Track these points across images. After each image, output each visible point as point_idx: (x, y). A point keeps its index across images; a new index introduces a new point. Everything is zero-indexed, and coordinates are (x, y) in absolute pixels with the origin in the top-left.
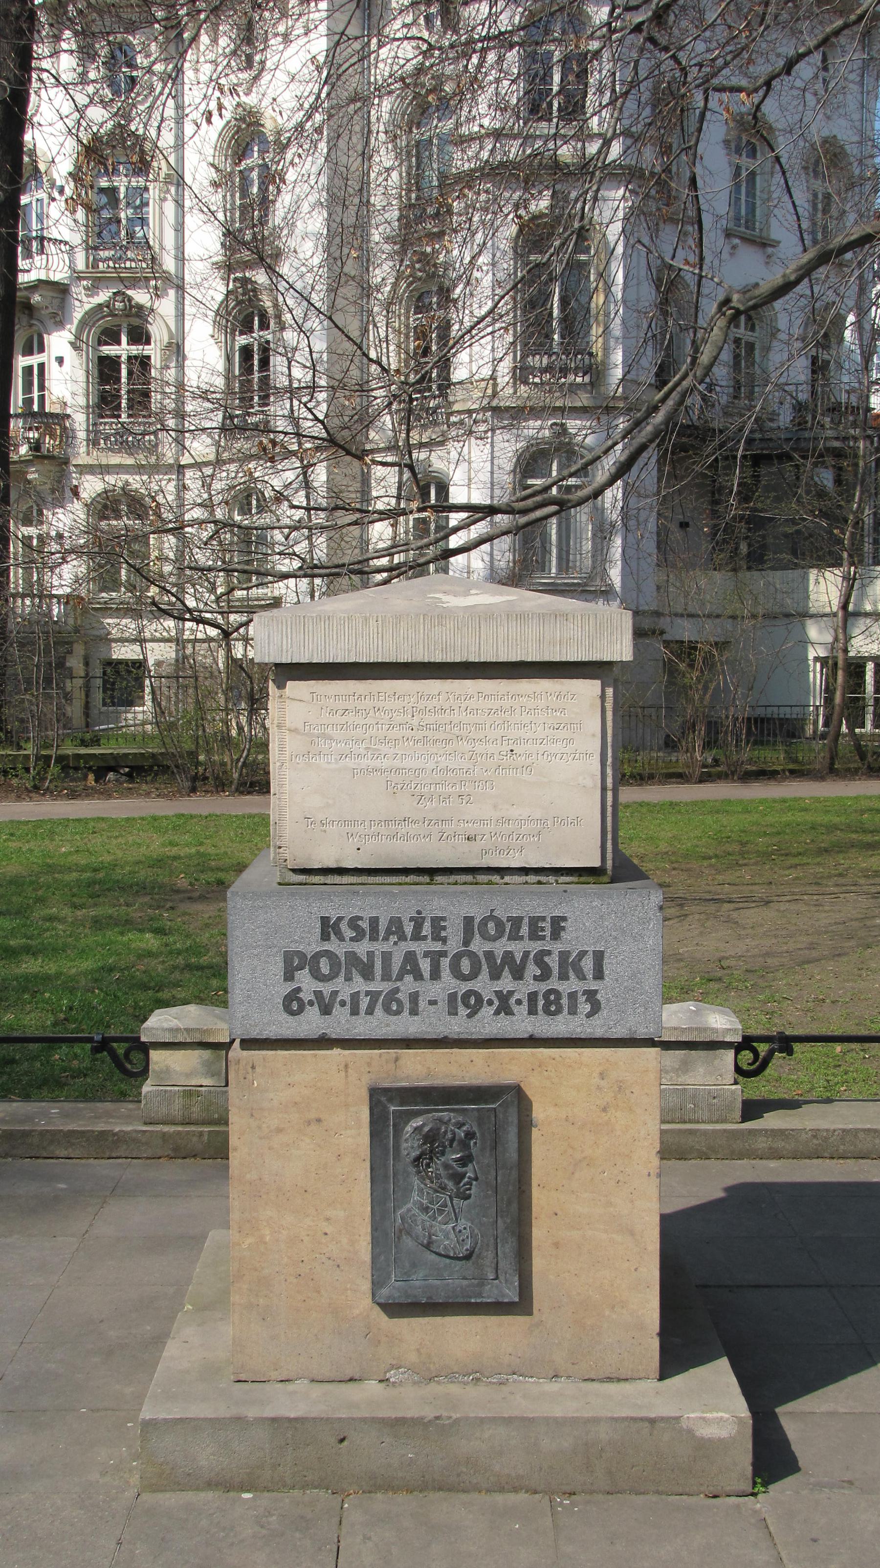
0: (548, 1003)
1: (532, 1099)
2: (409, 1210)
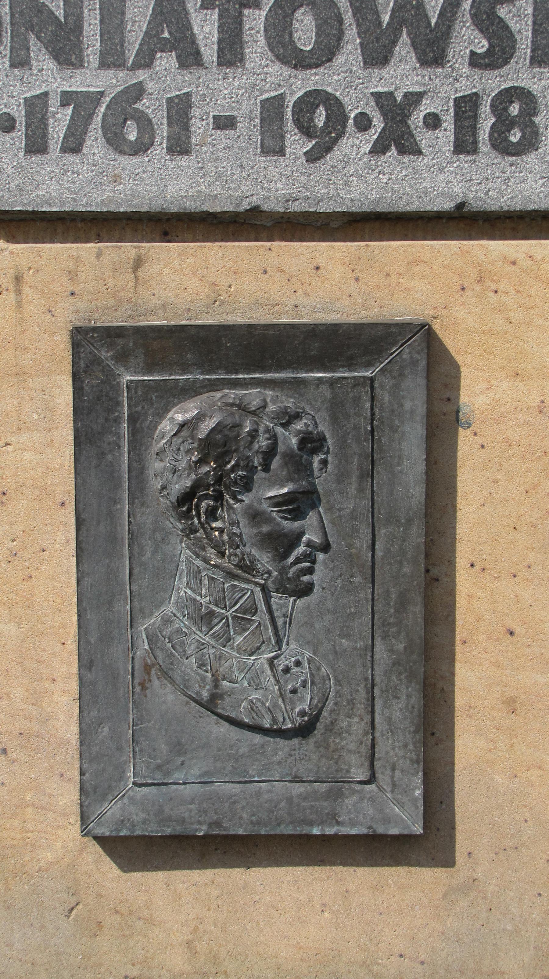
0: (503, 124)
1: (459, 359)
2: (167, 621)
